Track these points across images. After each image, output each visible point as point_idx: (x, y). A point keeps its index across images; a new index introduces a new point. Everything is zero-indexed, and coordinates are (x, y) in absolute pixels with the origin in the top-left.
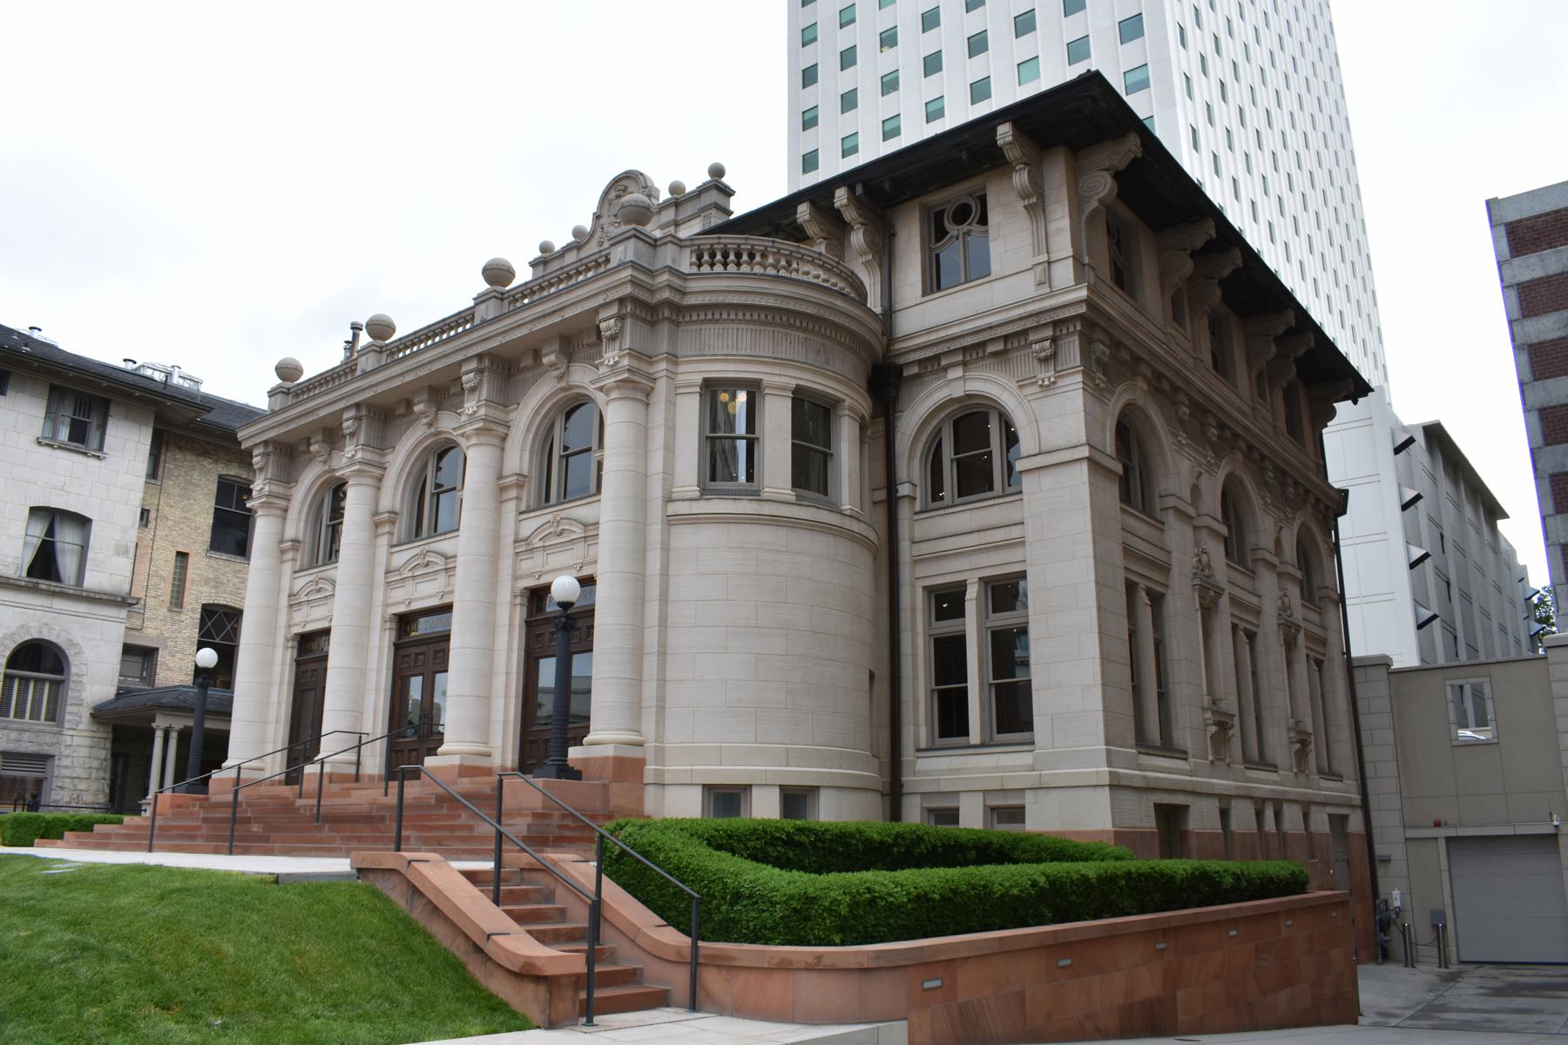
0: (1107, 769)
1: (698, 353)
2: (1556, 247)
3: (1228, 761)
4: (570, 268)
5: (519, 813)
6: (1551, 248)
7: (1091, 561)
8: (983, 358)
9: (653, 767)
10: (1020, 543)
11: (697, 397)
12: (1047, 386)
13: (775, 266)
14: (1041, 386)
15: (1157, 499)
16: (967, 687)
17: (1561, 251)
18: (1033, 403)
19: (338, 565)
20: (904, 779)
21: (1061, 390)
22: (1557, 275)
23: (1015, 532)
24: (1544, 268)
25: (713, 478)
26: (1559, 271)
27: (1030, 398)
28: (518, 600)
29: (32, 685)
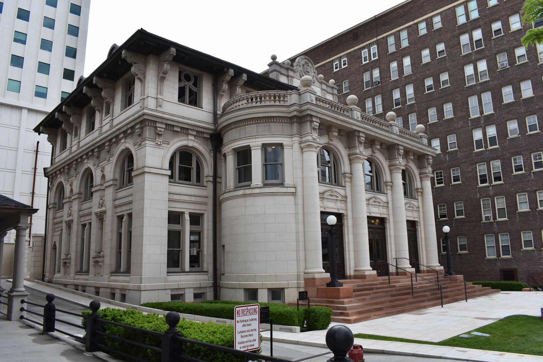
0: (296, 281)
1: (282, 134)
3: (69, 273)
4: (334, 103)
8: (200, 137)
9: (301, 281)
10: (130, 203)
11: (260, 150)
12: (159, 144)
13: (279, 101)
14: (156, 143)
19: (64, 210)
20: (213, 281)
23: (130, 199)
25: (266, 179)
28: (419, 224)
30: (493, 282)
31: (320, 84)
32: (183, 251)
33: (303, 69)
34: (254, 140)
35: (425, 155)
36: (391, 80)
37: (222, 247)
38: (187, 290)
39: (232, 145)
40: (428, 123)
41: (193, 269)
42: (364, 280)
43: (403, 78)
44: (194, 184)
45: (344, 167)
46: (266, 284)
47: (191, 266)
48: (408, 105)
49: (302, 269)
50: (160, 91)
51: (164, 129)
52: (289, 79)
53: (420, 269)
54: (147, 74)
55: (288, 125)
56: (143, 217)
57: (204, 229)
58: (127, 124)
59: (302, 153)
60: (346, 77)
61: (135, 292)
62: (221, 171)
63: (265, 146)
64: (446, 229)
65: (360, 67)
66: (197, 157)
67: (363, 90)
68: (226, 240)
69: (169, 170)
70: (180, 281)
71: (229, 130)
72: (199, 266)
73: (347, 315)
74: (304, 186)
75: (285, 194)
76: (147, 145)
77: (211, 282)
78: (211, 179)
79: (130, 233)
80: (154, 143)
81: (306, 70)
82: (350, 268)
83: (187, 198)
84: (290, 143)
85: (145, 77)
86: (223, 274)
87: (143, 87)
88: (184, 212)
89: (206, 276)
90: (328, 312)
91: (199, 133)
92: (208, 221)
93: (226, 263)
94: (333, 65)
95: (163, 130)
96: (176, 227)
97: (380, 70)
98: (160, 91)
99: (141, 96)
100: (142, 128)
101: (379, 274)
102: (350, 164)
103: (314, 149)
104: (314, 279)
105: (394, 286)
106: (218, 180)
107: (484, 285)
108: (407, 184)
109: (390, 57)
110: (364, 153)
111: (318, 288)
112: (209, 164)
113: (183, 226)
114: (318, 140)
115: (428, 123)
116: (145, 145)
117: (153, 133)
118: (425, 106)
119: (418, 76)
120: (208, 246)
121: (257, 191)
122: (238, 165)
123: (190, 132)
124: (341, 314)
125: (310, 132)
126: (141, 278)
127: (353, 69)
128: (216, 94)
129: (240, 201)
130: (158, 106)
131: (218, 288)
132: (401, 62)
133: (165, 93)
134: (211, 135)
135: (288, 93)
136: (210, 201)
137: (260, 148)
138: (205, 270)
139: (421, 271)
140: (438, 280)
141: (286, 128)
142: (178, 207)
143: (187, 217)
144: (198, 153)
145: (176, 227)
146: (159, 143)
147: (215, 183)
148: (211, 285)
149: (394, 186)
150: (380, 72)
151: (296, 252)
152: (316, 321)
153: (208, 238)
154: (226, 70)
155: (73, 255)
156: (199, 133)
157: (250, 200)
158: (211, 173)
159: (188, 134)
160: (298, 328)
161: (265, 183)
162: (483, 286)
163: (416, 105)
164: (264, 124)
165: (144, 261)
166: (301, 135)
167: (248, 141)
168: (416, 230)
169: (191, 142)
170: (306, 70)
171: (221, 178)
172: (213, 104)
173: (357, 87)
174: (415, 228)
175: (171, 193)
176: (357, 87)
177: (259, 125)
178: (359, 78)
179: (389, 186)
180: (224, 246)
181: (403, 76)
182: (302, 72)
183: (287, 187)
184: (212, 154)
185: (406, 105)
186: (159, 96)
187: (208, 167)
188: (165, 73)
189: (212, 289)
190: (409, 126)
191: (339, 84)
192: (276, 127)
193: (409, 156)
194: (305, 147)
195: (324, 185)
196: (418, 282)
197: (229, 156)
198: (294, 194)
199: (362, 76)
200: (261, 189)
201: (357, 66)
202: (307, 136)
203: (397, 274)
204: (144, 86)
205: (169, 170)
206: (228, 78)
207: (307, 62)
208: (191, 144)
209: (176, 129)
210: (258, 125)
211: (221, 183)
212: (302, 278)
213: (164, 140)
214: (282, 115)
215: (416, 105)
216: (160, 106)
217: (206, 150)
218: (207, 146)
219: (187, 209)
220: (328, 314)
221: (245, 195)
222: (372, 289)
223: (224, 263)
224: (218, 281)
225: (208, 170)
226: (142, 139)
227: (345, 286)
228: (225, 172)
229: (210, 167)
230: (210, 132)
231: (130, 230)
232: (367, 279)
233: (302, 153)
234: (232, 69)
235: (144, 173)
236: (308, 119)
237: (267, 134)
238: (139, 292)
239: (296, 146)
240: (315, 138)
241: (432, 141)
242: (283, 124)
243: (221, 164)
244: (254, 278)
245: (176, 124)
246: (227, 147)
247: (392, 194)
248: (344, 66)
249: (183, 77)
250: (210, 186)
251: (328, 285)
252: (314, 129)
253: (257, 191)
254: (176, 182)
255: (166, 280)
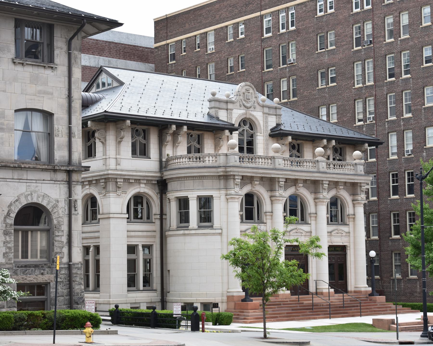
2: (94, 55)
5: (6, 239)
6: (93, 55)
7: (328, 274)
11: (196, 201)
15: (307, 215)
16: (99, 275)
17: (95, 58)
18: (102, 199)
21: (107, 197)
22: (93, 67)
23: (96, 235)
24: (90, 62)
26: (94, 66)
27: (101, 197)
29: (30, 233)
30: (417, 303)
31: (262, 108)
32: (138, 274)
33: (244, 97)
34: (191, 193)
35: (357, 183)
36: (385, 41)
37: (167, 272)
38: (141, 304)
39: (175, 194)
40: (423, 107)
41: (146, 288)
42: (277, 298)
43: (399, 42)
44: (145, 222)
45: (266, 207)
46: (199, 300)
47: (144, 286)
48: (402, 80)
49: (225, 289)
50: (118, 152)
51: (123, 182)
52: (228, 112)
53: (348, 290)
54: (108, 138)
55: (217, 180)
56: (110, 251)
57: (153, 257)
58: (92, 177)
59: (228, 202)
60: (332, 26)
61: (105, 305)
62: (166, 210)
63: (200, 198)
64: (373, 254)
65: (350, 16)
66: (147, 199)
67: (352, 50)
68: (171, 265)
69: (127, 213)
70: (137, 297)
71: (173, 181)
72: (150, 286)
73: (248, 319)
74: (228, 228)
75: (214, 234)
76: (111, 196)
77: (159, 298)
78: (158, 217)
79: (97, 262)
80: (116, 195)
81: (247, 97)
82: (351, 285)
83: (140, 234)
84: (218, 195)
85: (105, 141)
86: (169, 292)
87: (105, 148)
88: (138, 245)
89: (156, 293)
90: (230, 315)
91: (149, 182)
92: (156, 251)
93: (170, 284)
94: (316, 5)
95: (122, 183)
96: (133, 256)
97: (373, 25)
98: (118, 152)
99: (104, 155)
100: (105, 183)
101: (292, 294)
102: (272, 204)
103: (236, 200)
104: (233, 296)
105: (303, 303)
106: (164, 217)
107: (404, 306)
108: (338, 210)
109: (386, 9)
110: (284, 194)
111: (235, 303)
112: (157, 205)
113: (138, 255)
114: (240, 192)
115: (423, 107)
116: (109, 197)
117: (115, 186)
118: (421, 83)
119: (416, 42)
120: (156, 270)
121: (193, 232)
122: (180, 209)
123: (142, 181)
124: (245, 319)
125: (233, 187)
126: (110, 295)
127: (341, 17)
128: (161, 143)
129: (182, 238)
130: (117, 165)
131: (165, 303)
132: (398, 18)
133: (122, 152)
134: (158, 181)
135: (217, 155)
136: (158, 235)
137: (196, 199)
138: (155, 289)
139: (349, 291)
140: (343, 298)
141: (216, 183)
142: (133, 242)
143: (140, 248)
144: (147, 196)
145: (133, 256)
146: (119, 194)
147: (161, 219)
148: (159, 300)
149: (317, 217)
150: (373, 28)
151: (221, 277)
152: (223, 320)
153: (156, 264)
154: (169, 126)
155: (291, 308)
156: (149, 182)
157: (188, 239)
158: (158, 212)
159: (140, 183)
160: (211, 323)
161: (199, 225)
162: (403, 307)
163: (411, 80)
164: (198, 181)
165: (112, 283)
166: (226, 188)
167: (187, 193)
168: (346, 254)
169: (143, 189)
170: (247, 97)
171: (166, 215)
172: (159, 148)
173: (344, 43)
174: (345, 252)
175: (129, 230)
176: (344, 43)
177: (195, 181)
178: (348, 31)
179: (313, 217)
180: (169, 271)
181: (399, 39)
182: (243, 100)
183: (216, 229)
184: (159, 196)
185: (401, 78)
186: (118, 157)
187: (156, 206)
188: (122, 138)
189: (160, 304)
190: (403, 106)
191: (323, 34)
192: (207, 183)
193: (338, 186)
194: (229, 199)
195: (246, 224)
196: (331, 300)
197: (173, 202)
198: (221, 234)
199: (352, 29)
200: (196, 231)
201: (346, 14)
202: (231, 190)
203: (317, 293)
204: (106, 148)
205: (127, 213)
206: (171, 132)
207: (248, 89)
208: (142, 190)
209: (131, 181)
210: (194, 181)
211: (166, 219)
212: (225, 295)
213: (123, 191)
214: (212, 174)
215: (411, 80)
216: (119, 164)
217: (154, 193)
218: (155, 190)
219: (139, 242)
220: (230, 317)
221: (184, 235)
222: (280, 304)
223: (169, 283)
224: (164, 298)
225: (156, 209)
226: (106, 191)
227: (254, 302)
228: (169, 211)
229: (157, 207)
230: (157, 179)
231: (97, 258)
232: (280, 297)
233: (228, 202)
234: (174, 125)
235: (109, 218)
236: (232, 177)
237: (201, 188)
238: (109, 305)
239: (223, 197)
240: (237, 191)
241: (426, 129)
242: (214, 180)
243: (166, 202)
244: (191, 295)
245: (131, 178)
246: (171, 194)
247: (316, 224)
248: (330, 9)
249: (135, 133)
250: (158, 222)
251: (243, 300)
252: (236, 184)
253: (193, 232)
254: (132, 221)
255: (126, 297)
